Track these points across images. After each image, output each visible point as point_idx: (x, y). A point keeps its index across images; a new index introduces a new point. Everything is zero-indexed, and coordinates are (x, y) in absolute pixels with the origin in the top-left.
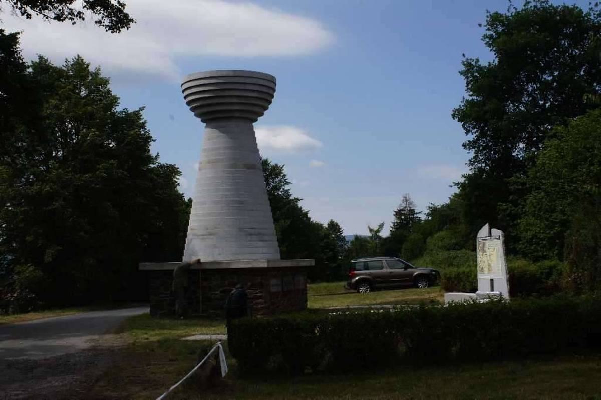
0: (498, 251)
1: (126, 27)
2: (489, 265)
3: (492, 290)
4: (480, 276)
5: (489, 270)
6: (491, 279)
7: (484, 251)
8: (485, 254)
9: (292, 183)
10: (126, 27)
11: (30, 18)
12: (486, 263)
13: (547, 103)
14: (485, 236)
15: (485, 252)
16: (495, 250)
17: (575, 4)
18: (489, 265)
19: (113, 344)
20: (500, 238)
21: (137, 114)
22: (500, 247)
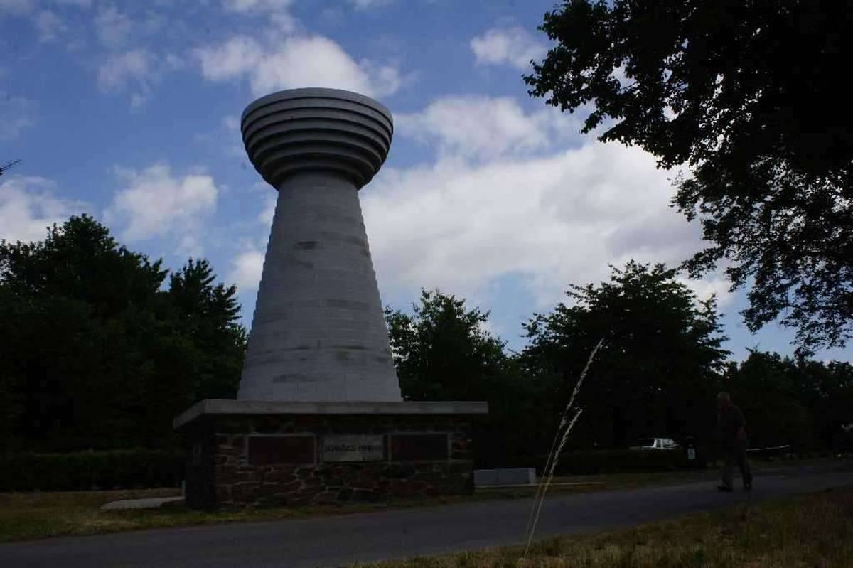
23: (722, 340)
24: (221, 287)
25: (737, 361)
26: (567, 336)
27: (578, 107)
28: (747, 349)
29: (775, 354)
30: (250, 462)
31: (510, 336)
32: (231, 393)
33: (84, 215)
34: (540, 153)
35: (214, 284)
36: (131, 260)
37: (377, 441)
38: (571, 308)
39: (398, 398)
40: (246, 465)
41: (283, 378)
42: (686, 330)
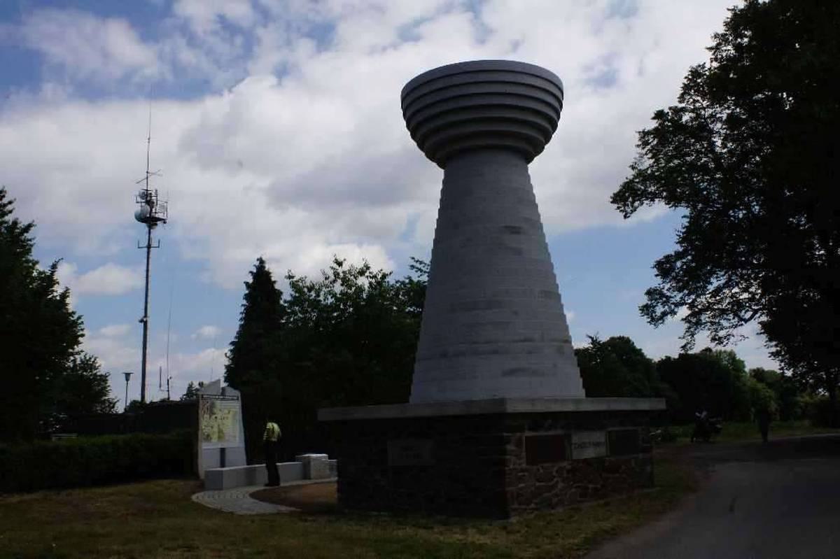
0: (234, 416)
1: (640, 143)
2: (220, 431)
3: (223, 465)
4: (204, 446)
5: (220, 438)
6: (221, 449)
7: (212, 413)
8: (214, 417)
9: (758, 334)
10: (640, 143)
11: (647, 310)
12: (216, 429)
13: (700, 242)
14: (215, 394)
15: (214, 414)
16: (231, 413)
17: (58, 283)
18: (220, 431)
19: (495, 396)
20: (238, 399)
21: (655, 266)
22: (238, 410)
23: (95, 360)
24: (15, 223)
25: (554, 49)
26: (31, 286)
27: (622, 336)
28: (728, 10)
29: (666, 357)
30: (528, 464)
31: (653, 362)
32: (402, 395)
33: (594, 342)
34: (157, 91)
35: (9, 218)
36: (659, 361)
37: (600, 437)
38: (144, 224)
39: (581, 393)
40: (524, 466)
41: (512, 372)
42: (4, 232)
